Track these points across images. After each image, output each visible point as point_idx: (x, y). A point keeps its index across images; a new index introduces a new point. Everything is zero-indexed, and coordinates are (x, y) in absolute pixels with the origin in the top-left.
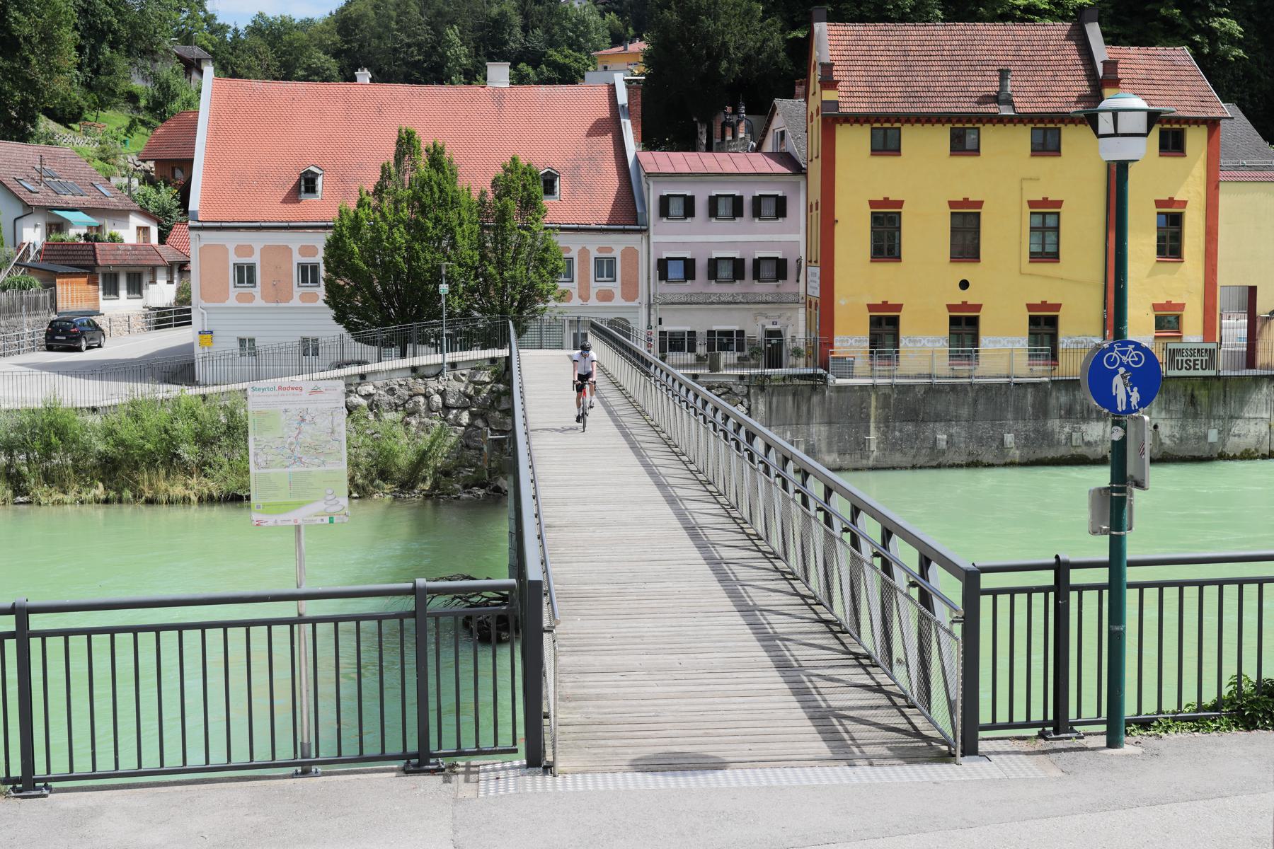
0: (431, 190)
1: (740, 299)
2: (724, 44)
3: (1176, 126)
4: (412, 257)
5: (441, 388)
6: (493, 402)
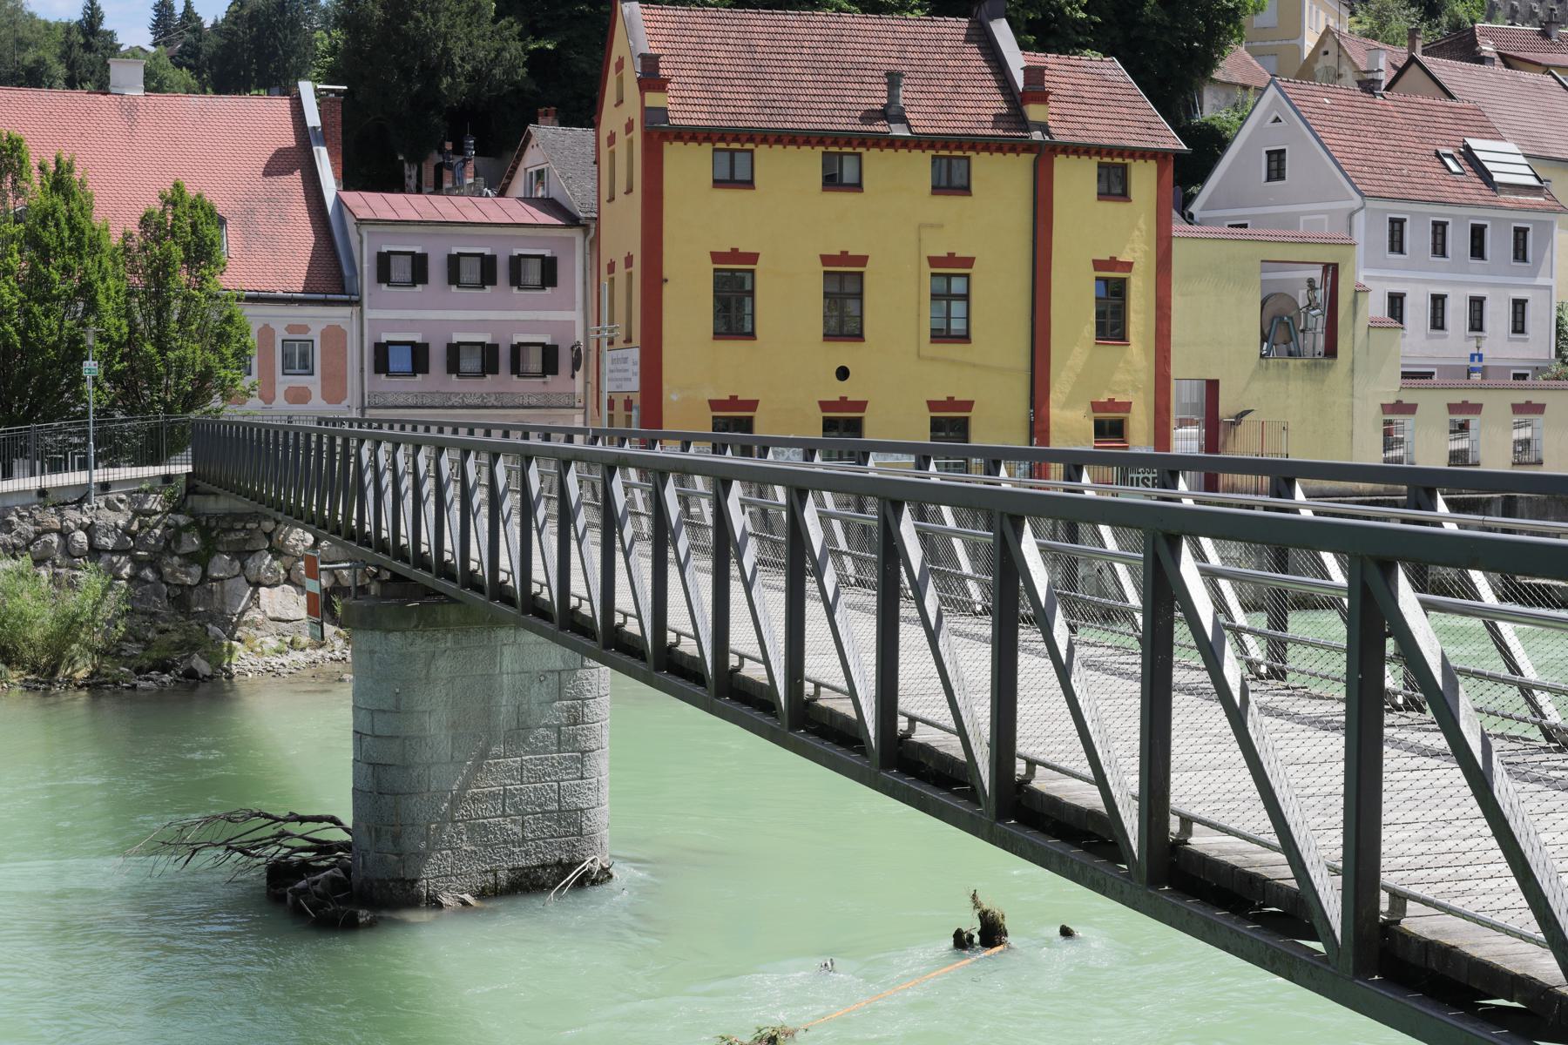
0: (57, 225)
1: (492, 401)
2: (446, 51)
3: (1118, 160)
4: (31, 324)
5: (87, 520)
6: (168, 542)
